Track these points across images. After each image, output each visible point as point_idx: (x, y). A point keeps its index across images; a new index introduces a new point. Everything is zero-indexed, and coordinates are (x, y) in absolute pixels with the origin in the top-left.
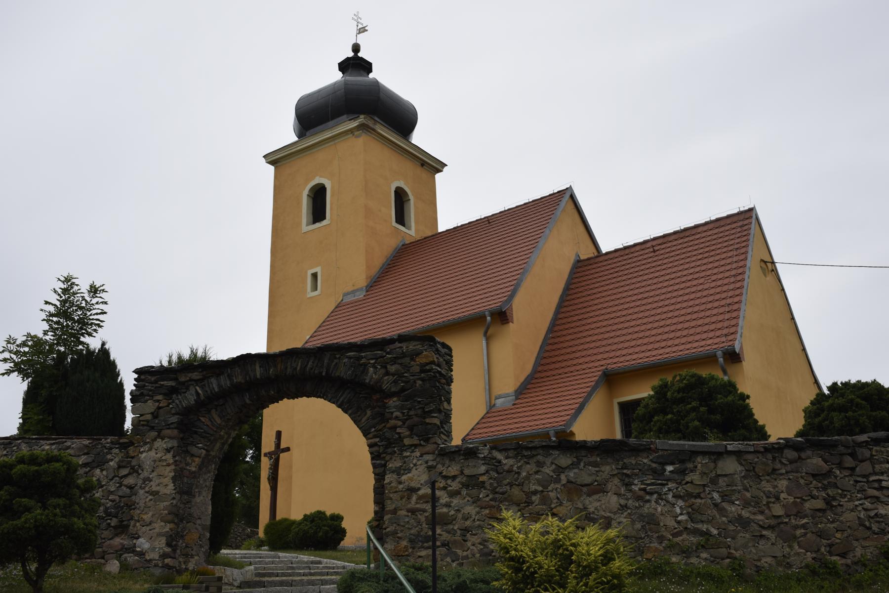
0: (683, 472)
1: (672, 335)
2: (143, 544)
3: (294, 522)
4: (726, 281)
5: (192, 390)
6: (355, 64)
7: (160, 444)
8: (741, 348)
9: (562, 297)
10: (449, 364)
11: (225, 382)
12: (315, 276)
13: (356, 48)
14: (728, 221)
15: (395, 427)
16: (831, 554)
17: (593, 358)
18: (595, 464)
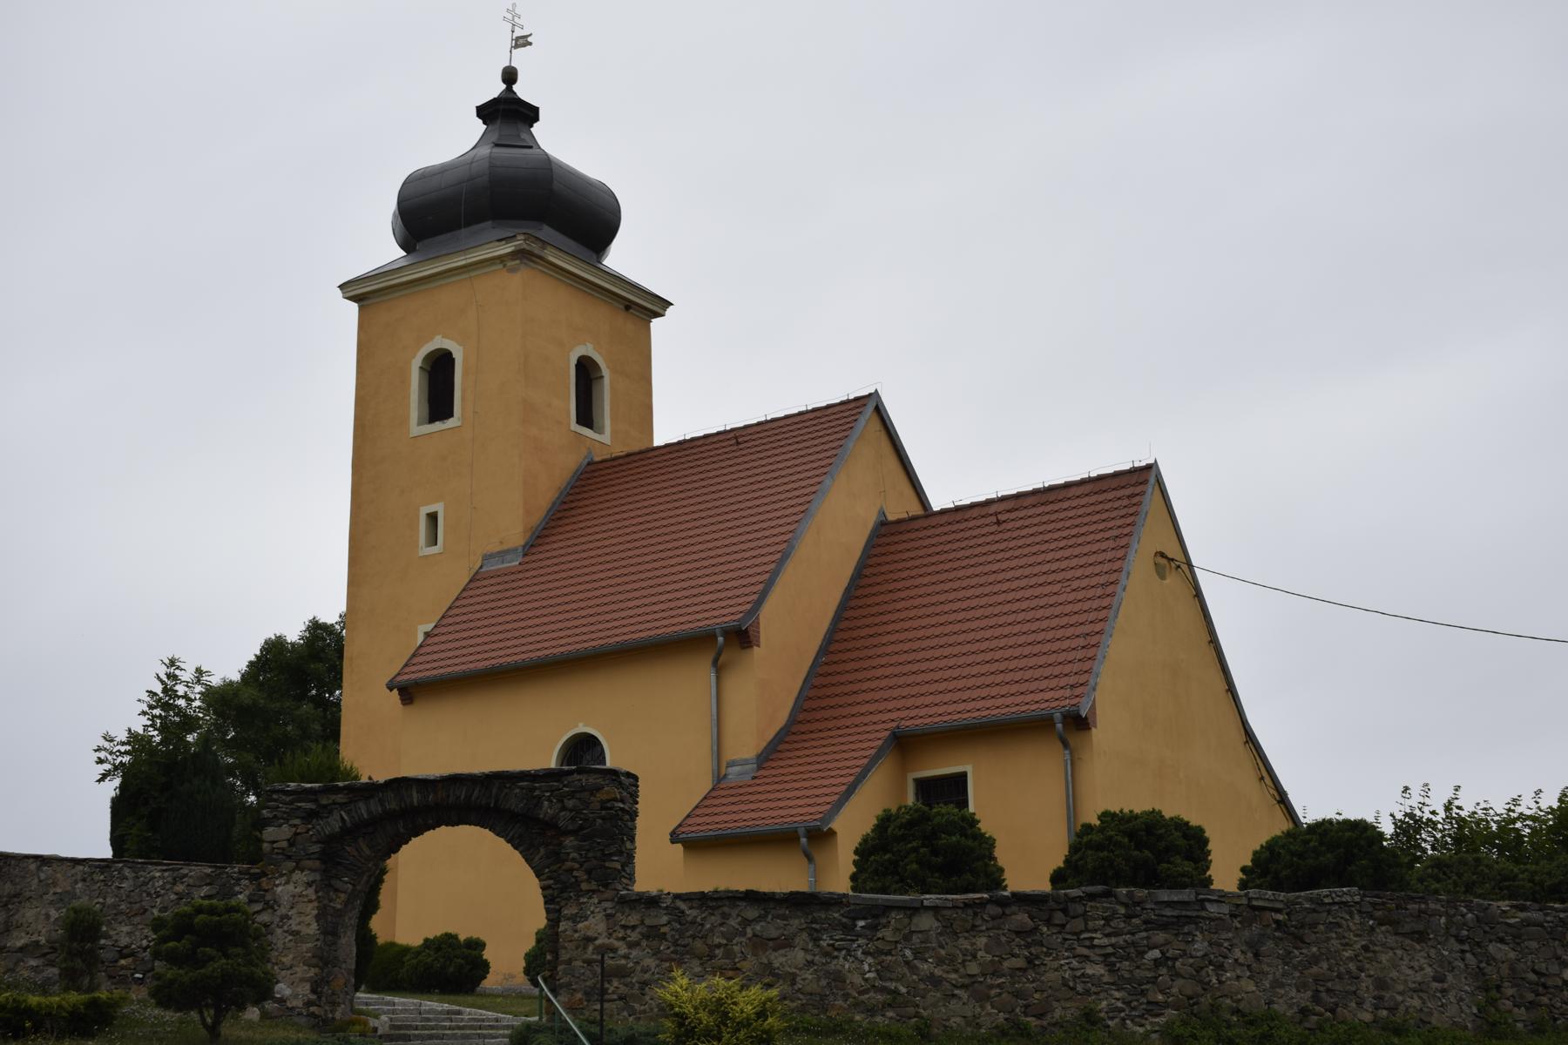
0: (874, 928)
3: (406, 950)
4: (1090, 593)
5: (336, 815)
6: (508, 114)
7: (298, 876)
9: (847, 590)
10: (634, 797)
11: (376, 808)
12: (433, 518)
13: (510, 76)
15: (571, 870)
16: (1026, 1015)
17: (882, 706)
18: (784, 918)
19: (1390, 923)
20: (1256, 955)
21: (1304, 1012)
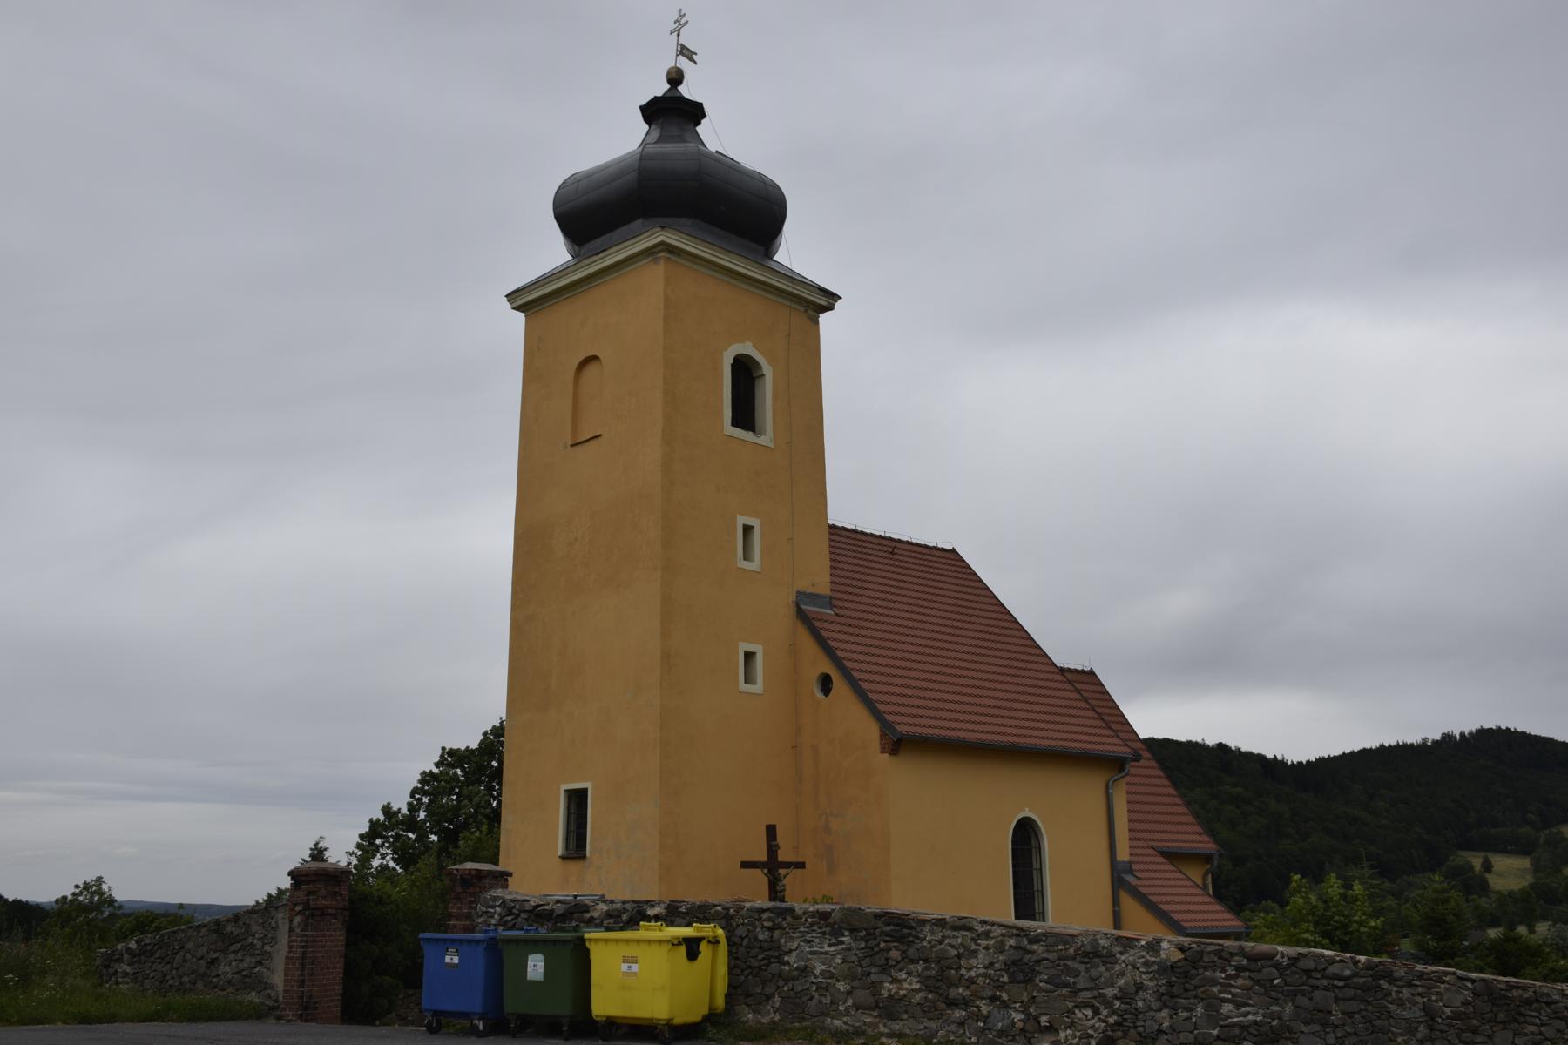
6: (673, 112)
13: (676, 78)
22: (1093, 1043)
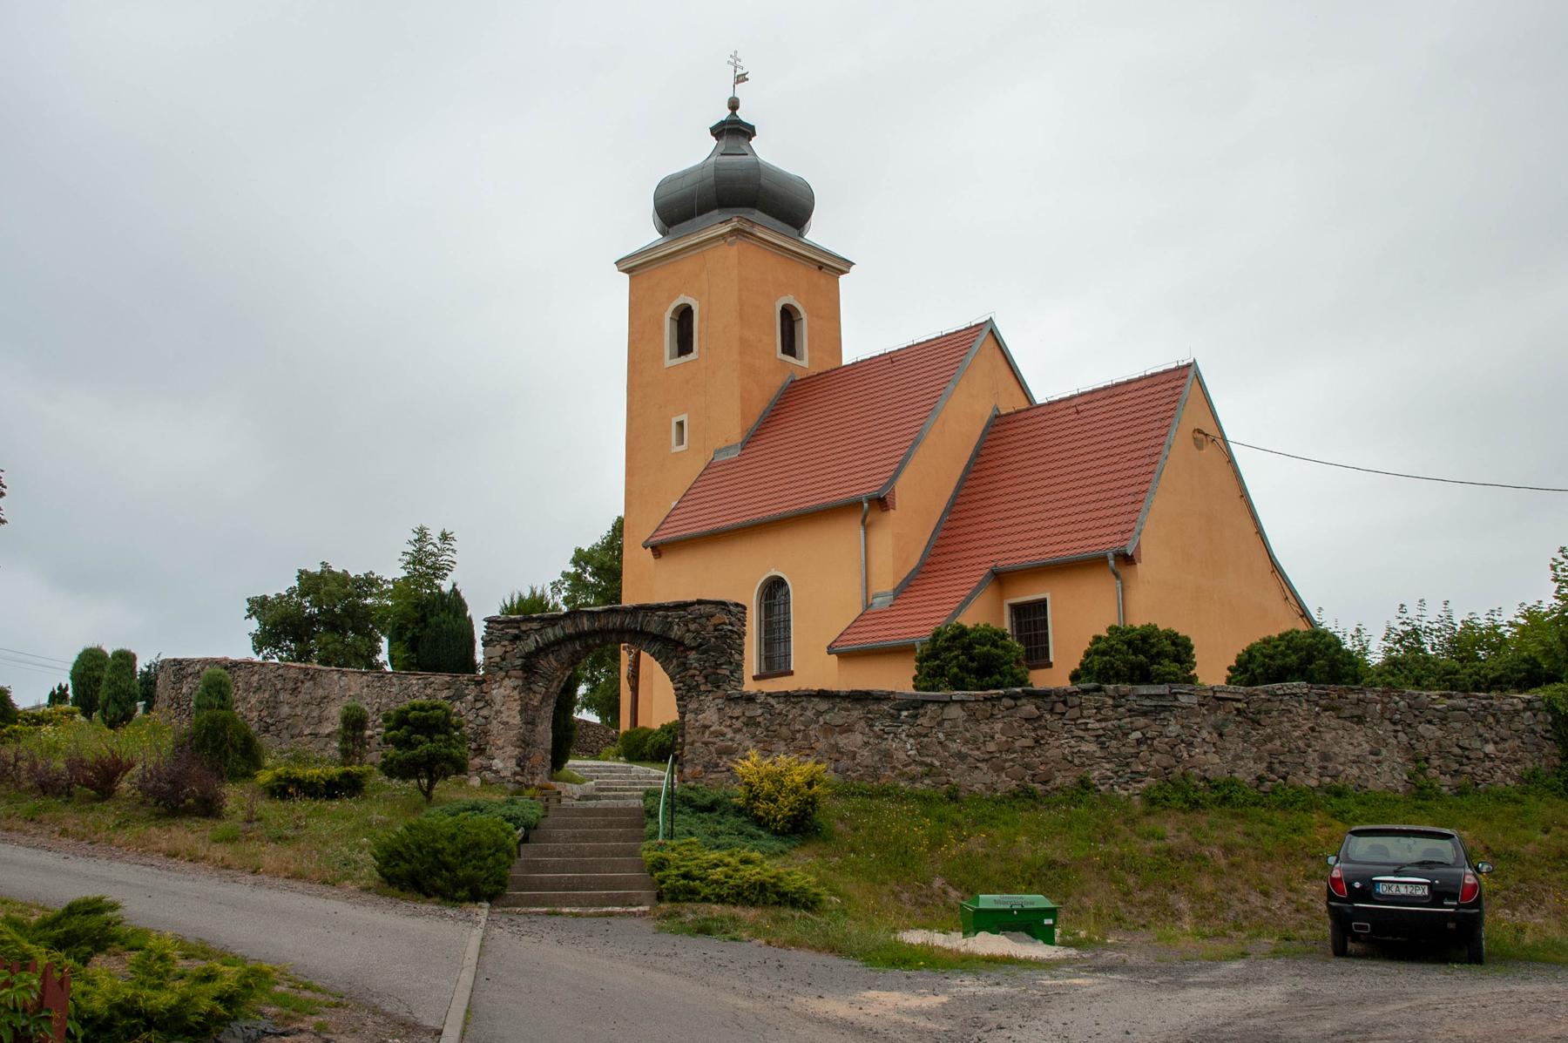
0: (915, 717)
1: (1071, 528)
2: (498, 764)
3: (651, 732)
5: (532, 637)
6: (733, 131)
8: (1138, 547)
11: (559, 632)
12: (680, 424)
13: (734, 105)
14: (1163, 378)
18: (847, 710)
19: (1333, 709)
20: (1221, 735)
21: (1260, 779)
22: (1566, 591)
